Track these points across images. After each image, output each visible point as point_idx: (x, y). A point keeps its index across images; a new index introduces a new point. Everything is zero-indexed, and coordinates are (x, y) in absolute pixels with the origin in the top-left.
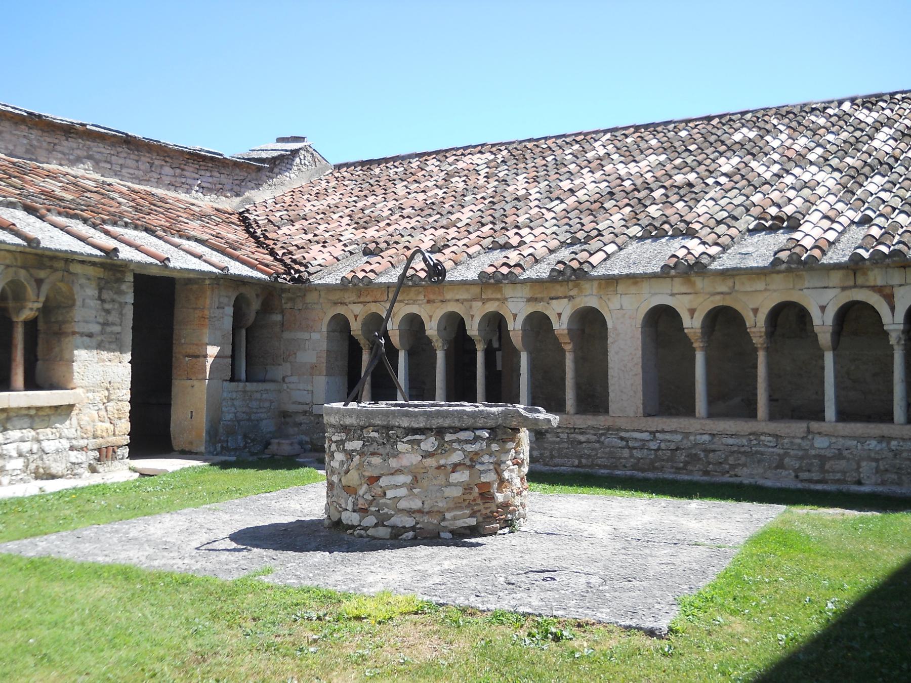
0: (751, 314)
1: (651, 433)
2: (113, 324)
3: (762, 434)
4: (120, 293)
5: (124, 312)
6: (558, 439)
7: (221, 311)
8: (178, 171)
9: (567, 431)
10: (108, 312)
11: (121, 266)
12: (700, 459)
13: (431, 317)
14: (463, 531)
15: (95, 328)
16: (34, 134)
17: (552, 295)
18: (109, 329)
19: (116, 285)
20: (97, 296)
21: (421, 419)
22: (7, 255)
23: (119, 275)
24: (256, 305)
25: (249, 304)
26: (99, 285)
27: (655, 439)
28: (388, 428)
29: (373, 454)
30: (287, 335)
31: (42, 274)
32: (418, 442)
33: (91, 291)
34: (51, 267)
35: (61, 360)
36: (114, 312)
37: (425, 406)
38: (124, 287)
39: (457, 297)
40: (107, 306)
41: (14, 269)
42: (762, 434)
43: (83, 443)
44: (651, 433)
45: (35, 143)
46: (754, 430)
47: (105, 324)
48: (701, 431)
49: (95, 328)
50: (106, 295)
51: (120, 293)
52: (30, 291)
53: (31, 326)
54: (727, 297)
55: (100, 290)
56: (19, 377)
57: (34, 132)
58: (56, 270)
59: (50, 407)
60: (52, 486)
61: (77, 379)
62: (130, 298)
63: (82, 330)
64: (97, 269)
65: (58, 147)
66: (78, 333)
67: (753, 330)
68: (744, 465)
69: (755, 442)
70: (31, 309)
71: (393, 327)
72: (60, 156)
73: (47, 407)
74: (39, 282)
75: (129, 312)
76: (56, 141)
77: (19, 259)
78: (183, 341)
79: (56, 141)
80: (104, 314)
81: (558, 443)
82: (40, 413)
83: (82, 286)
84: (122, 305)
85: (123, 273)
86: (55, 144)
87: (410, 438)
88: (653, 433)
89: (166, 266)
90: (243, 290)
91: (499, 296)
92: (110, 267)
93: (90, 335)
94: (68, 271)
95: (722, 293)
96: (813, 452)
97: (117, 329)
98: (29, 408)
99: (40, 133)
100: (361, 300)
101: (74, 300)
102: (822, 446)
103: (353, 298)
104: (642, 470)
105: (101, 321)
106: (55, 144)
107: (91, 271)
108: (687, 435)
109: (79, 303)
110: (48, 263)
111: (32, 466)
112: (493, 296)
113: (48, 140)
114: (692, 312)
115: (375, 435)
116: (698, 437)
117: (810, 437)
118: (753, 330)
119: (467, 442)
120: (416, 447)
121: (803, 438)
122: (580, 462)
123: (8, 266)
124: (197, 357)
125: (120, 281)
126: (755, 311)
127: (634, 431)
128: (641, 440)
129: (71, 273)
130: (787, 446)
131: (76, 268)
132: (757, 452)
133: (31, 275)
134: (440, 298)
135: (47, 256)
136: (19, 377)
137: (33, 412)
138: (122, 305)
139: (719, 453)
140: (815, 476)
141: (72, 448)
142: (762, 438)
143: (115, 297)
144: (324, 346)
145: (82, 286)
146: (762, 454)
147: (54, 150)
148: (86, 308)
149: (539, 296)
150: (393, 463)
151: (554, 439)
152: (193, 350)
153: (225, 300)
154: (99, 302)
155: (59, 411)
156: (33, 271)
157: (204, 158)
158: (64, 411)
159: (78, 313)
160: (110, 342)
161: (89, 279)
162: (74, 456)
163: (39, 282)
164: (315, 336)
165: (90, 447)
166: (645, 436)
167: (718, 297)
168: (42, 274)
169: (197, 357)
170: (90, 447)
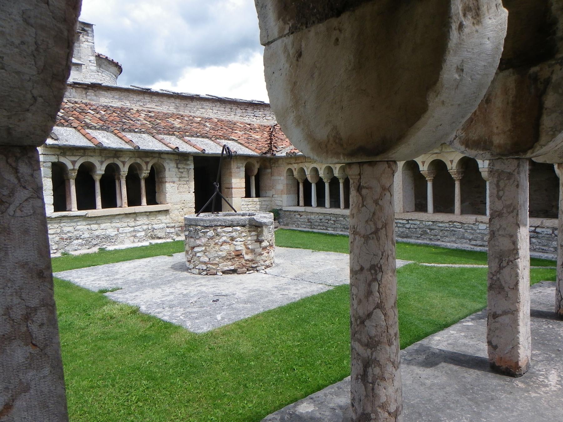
0: (450, 163)
1: (407, 220)
2: (184, 177)
3: (455, 222)
8: (244, 111)
12: (428, 233)
14: (231, 272)
16: (178, 101)
23: (186, 158)
24: (257, 166)
25: (254, 166)
27: (408, 223)
30: (273, 178)
31: (148, 160)
34: (152, 156)
37: (308, 209)
38: (189, 162)
42: (455, 222)
43: (173, 225)
44: (407, 220)
45: (178, 105)
46: (451, 220)
50: (180, 166)
52: (145, 168)
54: (439, 155)
55: (177, 164)
56: (144, 201)
57: (177, 100)
58: (155, 157)
61: (168, 199)
62: (192, 167)
65: (188, 105)
67: (451, 171)
68: (446, 236)
69: (452, 226)
71: (308, 172)
72: (189, 109)
74: (147, 163)
84: (188, 170)
88: (408, 220)
89: (204, 153)
90: (249, 160)
95: (436, 153)
96: (478, 231)
98: (146, 212)
102: (482, 228)
103: (294, 161)
104: (403, 237)
108: (421, 221)
111: (149, 234)
114: (423, 163)
117: (477, 224)
118: (451, 171)
119: (230, 232)
121: (473, 224)
126: (452, 161)
127: (399, 219)
128: (403, 224)
130: (466, 228)
132: (452, 230)
136: (144, 201)
140: (479, 243)
141: (168, 227)
142: (455, 224)
144: (285, 182)
146: (455, 231)
147: (186, 106)
150: (198, 242)
152: (227, 186)
157: (256, 104)
158: (166, 212)
162: (168, 230)
164: (282, 178)
165: (176, 226)
166: (404, 222)
167: (435, 155)
170: (176, 226)
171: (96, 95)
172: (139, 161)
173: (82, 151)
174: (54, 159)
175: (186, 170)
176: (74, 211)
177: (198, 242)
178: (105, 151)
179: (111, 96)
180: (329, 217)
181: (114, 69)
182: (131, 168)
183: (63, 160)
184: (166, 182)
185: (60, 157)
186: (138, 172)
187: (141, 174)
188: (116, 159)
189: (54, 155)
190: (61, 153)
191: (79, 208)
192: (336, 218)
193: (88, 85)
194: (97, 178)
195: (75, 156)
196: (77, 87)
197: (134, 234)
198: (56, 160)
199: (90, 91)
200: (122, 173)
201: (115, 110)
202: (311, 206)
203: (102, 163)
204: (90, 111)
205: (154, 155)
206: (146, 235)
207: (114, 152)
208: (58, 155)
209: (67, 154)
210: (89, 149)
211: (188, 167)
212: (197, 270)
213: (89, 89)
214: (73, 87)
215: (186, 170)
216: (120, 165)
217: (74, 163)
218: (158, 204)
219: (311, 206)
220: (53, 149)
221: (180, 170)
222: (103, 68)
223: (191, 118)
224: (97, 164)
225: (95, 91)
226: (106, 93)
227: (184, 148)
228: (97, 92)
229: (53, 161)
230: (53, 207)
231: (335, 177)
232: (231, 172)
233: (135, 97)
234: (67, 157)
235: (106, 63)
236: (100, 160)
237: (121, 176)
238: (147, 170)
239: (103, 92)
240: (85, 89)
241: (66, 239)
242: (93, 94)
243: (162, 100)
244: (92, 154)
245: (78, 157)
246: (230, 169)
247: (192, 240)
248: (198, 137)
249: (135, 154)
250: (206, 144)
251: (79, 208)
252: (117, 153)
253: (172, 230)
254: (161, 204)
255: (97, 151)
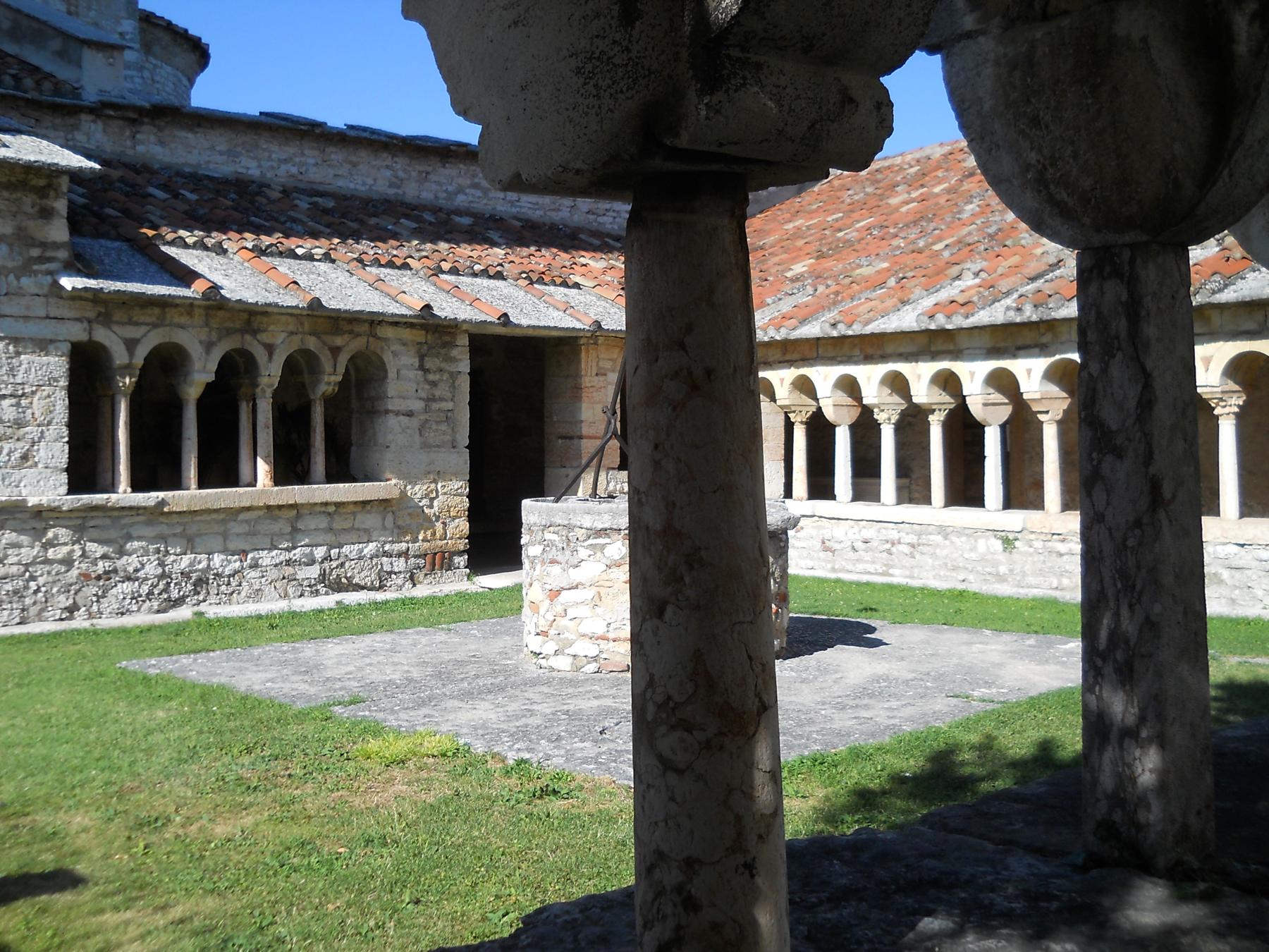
2: (442, 399)
4: (454, 360)
5: (457, 383)
6: (1031, 550)
7: (602, 378)
9: (1043, 537)
10: (434, 384)
11: (449, 326)
13: (869, 378)
15: (418, 405)
17: (1020, 342)
18: (435, 406)
19: (443, 351)
20: (417, 365)
21: (606, 517)
22: (290, 319)
23: (447, 338)
26: (418, 351)
28: (570, 528)
29: (553, 562)
31: (339, 341)
32: (603, 546)
33: (409, 360)
34: (351, 332)
35: (375, 445)
36: (442, 385)
38: (455, 353)
39: (901, 350)
40: (431, 377)
41: (300, 336)
45: (401, 174)
47: (430, 400)
48: (1222, 540)
49: (418, 405)
51: (454, 360)
52: (327, 365)
53: (329, 401)
55: (422, 358)
56: (319, 463)
58: (358, 335)
59: (355, 503)
60: (351, 598)
62: (465, 366)
63: (396, 408)
64: (415, 332)
65: (432, 177)
66: (392, 411)
70: (329, 383)
73: (349, 503)
74: (335, 351)
75: (465, 384)
76: (430, 169)
77: (306, 325)
78: (555, 418)
79: (430, 169)
80: (427, 387)
81: (1031, 555)
82: (342, 510)
83: (395, 354)
84: (454, 376)
85: (453, 335)
86: (428, 173)
87: (591, 541)
91: (951, 347)
92: (430, 329)
93: (410, 414)
94: (375, 336)
97: (450, 405)
98: (326, 504)
99: (407, 160)
100: (787, 358)
101: (386, 372)
105: (424, 395)
106: (428, 173)
107: (406, 334)
109: (392, 374)
110: (347, 327)
112: (944, 347)
113: (421, 168)
115: (555, 537)
116: (1219, 548)
120: (599, 554)
122: (1060, 583)
123: (292, 333)
124: (571, 438)
125: (451, 345)
129: (379, 338)
131: (389, 332)
133: (324, 343)
134: (879, 352)
135: (344, 319)
136: (319, 463)
137: (332, 509)
138: (454, 376)
139: (1249, 573)
143: (443, 365)
145: (395, 354)
148: (403, 383)
149: (1002, 345)
150: (576, 575)
151: (1027, 548)
153: (608, 365)
154: (420, 372)
155: (368, 507)
156: (324, 337)
159: (393, 387)
160: (438, 423)
161: (404, 344)
163: (335, 351)
168: (339, 341)
169: (571, 438)
171: (161, 143)
172: (312, 343)
173: (157, 311)
174: (78, 333)
175: (445, 376)
176: (124, 495)
177: (576, 575)
178: (221, 313)
179: (223, 147)
180: (894, 535)
181: (193, 57)
182: (290, 366)
183: (102, 335)
184: (387, 412)
185: (95, 326)
186: (307, 378)
187: (317, 382)
188: (248, 337)
189: (79, 320)
190: (100, 314)
191: (136, 486)
192: (919, 535)
193: (141, 111)
194: (192, 392)
195: (137, 324)
196: (110, 117)
197: (289, 571)
198: (83, 337)
199: (145, 128)
200: (264, 381)
201: (955, 243)
202: (832, 496)
203: (209, 346)
204: (152, 190)
205: (357, 329)
206: (323, 577)
207: (245, 316)
208: (90, 321)
209: (116, 318)
210: (177, 306)
211: (453, 368)
212: (570, 659)
213: (142, 123)
214: (99, 116)
215: (445, 376)
216: (260, 354)
217: (131, 345)
218: (354, 480)
219: (832, 496)
220: (78, 303)
221: (431, 377)
222: (155, 57)
223: (442, 215)
224: (195, 350)
225: (160, 129)
226: (190, 135)
227: (447, 308)
228: (167, 132)
229: (74, 339)
230: (64, 477)
231: (917, 406)
232: (578, 388)
233: (275, 148)
234: (115, 328)
235: (167, 38)
236: (204, 337)
237: (258, 390)
238: (334, 373)
239: (183, 134)
240: (133, 122)
241: (99, 578)
242: (153, 138)
243: (353, 158)
244: (183, 320)
245: (143, 329)
246: (577, 375)
247: (556, 569)
248: (475, 275)
249: (302, 324)
250: (507, 298)
251: (136, 486)
252: (252, 317)
253: (400, 564)
254: (367, 478)
255: (197, 311)
